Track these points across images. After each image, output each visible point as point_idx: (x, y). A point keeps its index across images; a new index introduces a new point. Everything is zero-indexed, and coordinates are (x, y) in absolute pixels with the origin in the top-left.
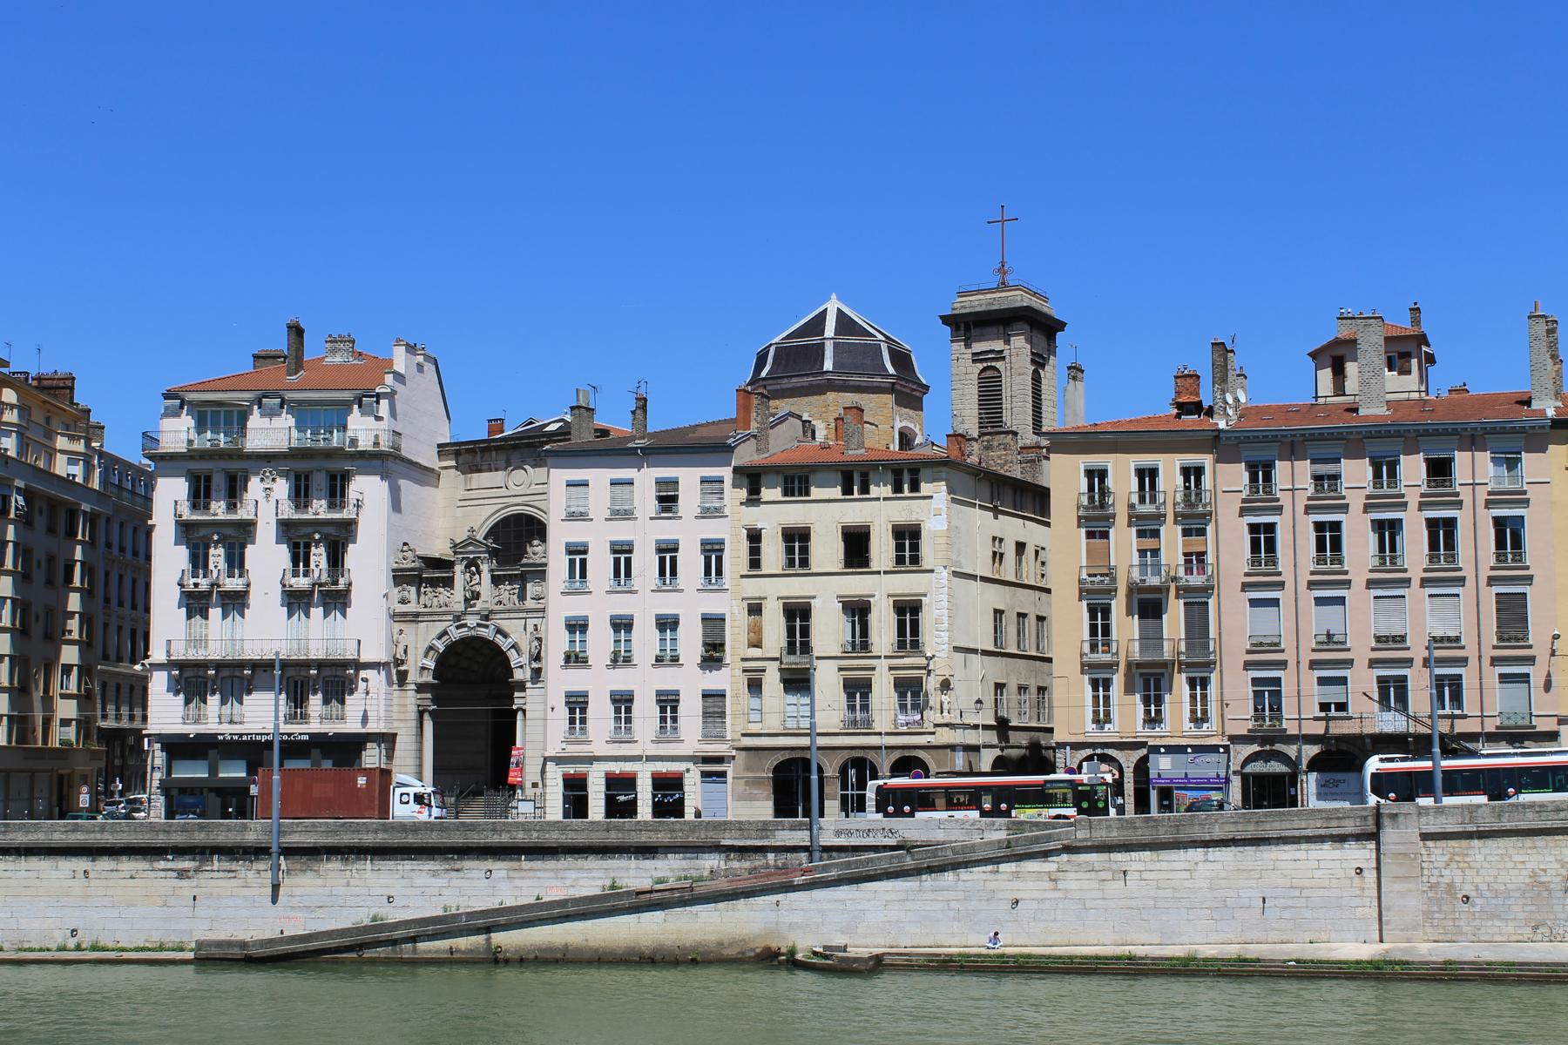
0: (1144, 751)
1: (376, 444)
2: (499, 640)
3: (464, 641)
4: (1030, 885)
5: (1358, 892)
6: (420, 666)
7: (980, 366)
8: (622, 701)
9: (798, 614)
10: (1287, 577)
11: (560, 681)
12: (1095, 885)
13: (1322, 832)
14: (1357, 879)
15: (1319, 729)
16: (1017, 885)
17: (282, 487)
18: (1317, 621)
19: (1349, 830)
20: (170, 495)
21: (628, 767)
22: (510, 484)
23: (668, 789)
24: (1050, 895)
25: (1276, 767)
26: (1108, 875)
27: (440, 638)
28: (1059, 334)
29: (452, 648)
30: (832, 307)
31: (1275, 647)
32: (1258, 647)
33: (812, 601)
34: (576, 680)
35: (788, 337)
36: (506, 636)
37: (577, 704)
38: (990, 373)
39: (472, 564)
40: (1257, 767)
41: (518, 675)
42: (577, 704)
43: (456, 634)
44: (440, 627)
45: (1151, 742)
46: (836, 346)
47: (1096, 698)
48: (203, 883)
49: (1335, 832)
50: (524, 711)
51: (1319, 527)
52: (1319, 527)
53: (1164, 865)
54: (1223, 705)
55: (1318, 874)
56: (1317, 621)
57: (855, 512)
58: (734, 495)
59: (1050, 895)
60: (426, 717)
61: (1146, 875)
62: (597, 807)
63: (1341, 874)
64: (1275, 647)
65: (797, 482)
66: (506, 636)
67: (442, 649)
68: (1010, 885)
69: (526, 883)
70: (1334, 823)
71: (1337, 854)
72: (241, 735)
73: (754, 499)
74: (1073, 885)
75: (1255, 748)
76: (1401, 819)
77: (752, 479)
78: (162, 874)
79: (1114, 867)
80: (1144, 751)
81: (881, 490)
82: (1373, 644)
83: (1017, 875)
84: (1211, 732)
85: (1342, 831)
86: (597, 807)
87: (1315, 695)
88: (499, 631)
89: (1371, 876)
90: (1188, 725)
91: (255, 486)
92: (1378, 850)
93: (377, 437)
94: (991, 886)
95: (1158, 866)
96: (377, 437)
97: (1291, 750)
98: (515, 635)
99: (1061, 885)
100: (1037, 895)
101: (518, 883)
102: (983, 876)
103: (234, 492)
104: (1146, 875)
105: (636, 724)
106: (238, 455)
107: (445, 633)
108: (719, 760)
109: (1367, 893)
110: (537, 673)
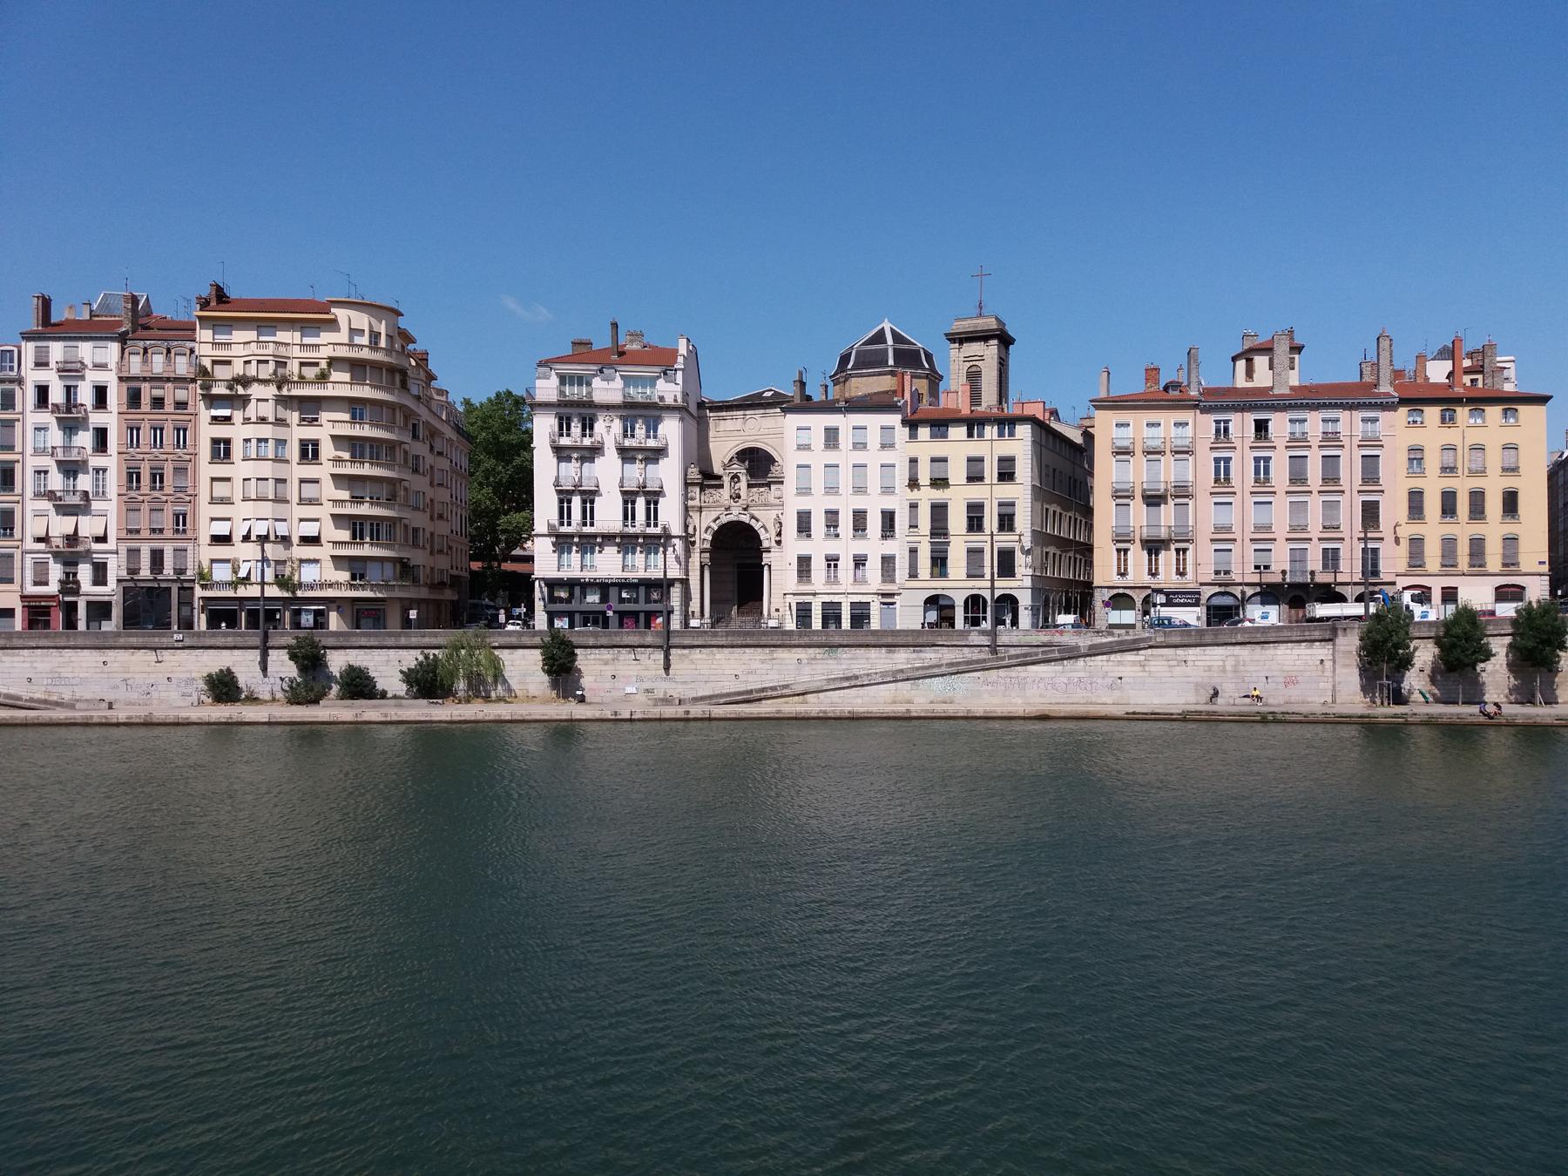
0: (1149, 591)
1: (676, 401)
2: (753, 523)
3: (731, 523)
4: (1129, 669)
5: (1320, 673)
6: (703, 538)
7: (968, 364)
8: (832, 561)
9: (939, 511)
10: (1237, 489)
11: (794, 546)
12: (1166, 669)
13: (1301, 638)
14: (1320, 667)
15: (1256, 579)
16: (1121, 668)
17: (617, 426)
18: (1253, 516)
19: (1317, 638)
20: (543, 427)
21: (836, 599)
22: (746, 429)
23: (860, 615)
24: (1140, 674)
25: (1228, 601)
26: (1174, 663)
27: (715, 521)
28: (1011, 347)
29: (723, 527)
30: (887, 326)
31: (1268, 528)
32: (1218, 529)
33: (949, 502)
34: (804, 547)
35: (863, 344)
36: (757, 520)
37: (804, 563)
38: (973, 369)
39: (735, 478)
40: (1217, 601)
41: (765, 544)
42: (804, 563)
43: (724, 520)
44: (714, 515)
45: (1153, 586)
46: (895, 350)
47: (1178, 560)
48: (620, 667)
49: (1308, 638)
50: (770, 566)
51: (1257, 460)
52: (1257, 460)
53: (1208, 658)
54: (1197, 564)
55: (1298, 663)
56: (1232, 517)
57: (976, 448)
58: (902, 433)
59: (1140, 674)
60: (706, 567)
61: (1196, 663)
62: (817, 623)
63: (1311, 663)
64: (1228, 529)
65: (940, 425)
66: (757, 520)
67: (716, 528)
68: (1116, 669)
69: (820, 667)
70: (1307, 633)
71: (1308, 651)
72: (595, 579)
73: (913, 436)
74: (1153, 669)
75: (1217, 589)
76: (1348, 631)
77: (912, 424)
78: (593, 662)
79: (1179, 658)
80: (1149, 591)
81: (990, 431)
82: (1321, 529)
83: (1120, 663)
84: (1189, 581)
85: (1313, 638)
86: (817, 623)
87: (1251, 559)
88: (753, 517)
89: (1328, 664)
90: (1175, 577)
91: (599, 426)
92: (1334, 649)
93: (675, 396)
94: (1105, 669)
95: (1204, 658)
96: (675, 396)
97: (1237, 591)
98: (764, 522)
99: (1147, 669)
100: (1132, 674)
101: (814, 667)
102: (1100, 663)
103: (588, 425)
104: (1196, 663)
105: (841, 573)
106: (591, 404)
107: (719, 518)
108: (892, 595)
109: (1326, 674)
110: (779, 543)
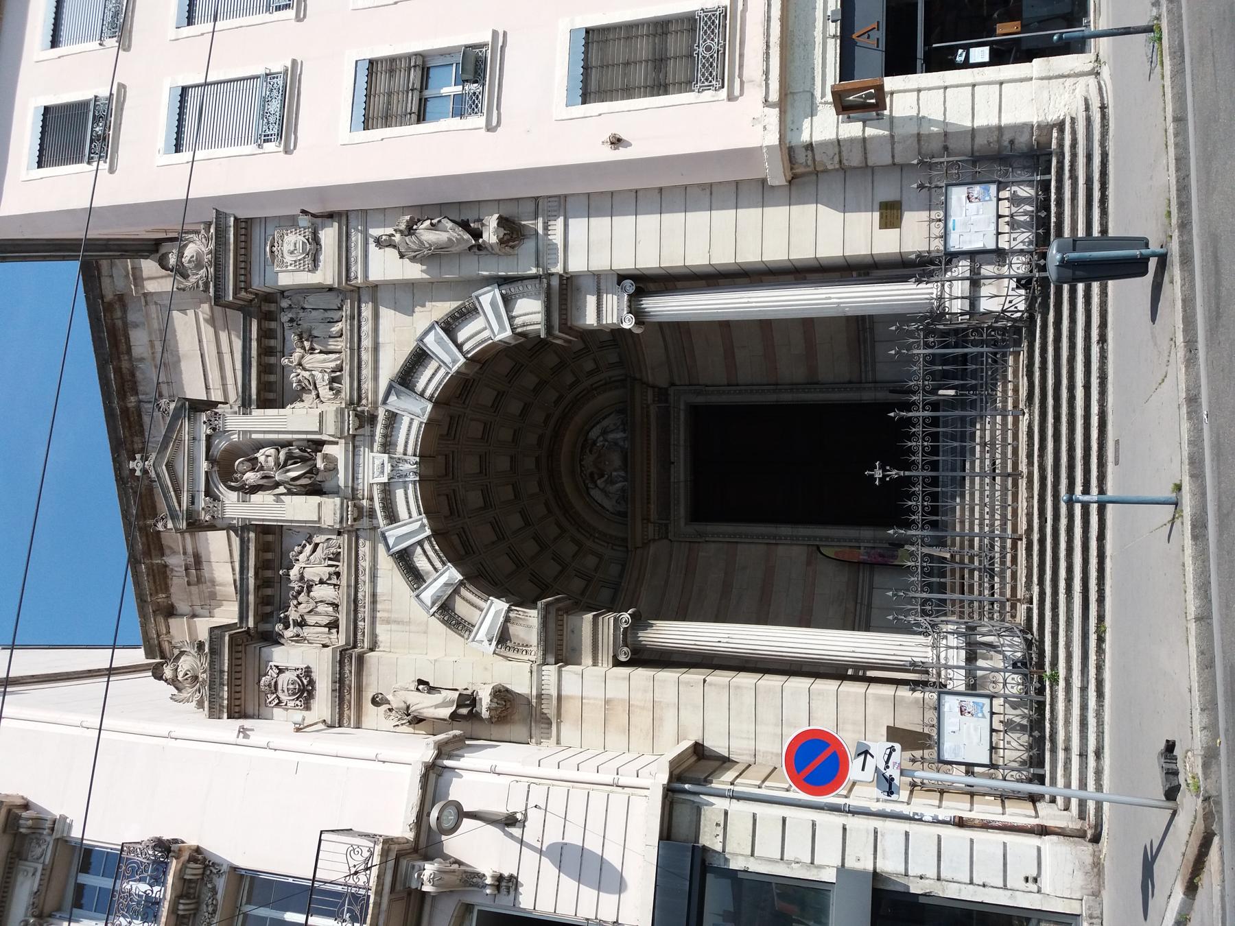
2: (430, 380)
27: (415, 577)
67: (453, 574)
88: (405, 379)
